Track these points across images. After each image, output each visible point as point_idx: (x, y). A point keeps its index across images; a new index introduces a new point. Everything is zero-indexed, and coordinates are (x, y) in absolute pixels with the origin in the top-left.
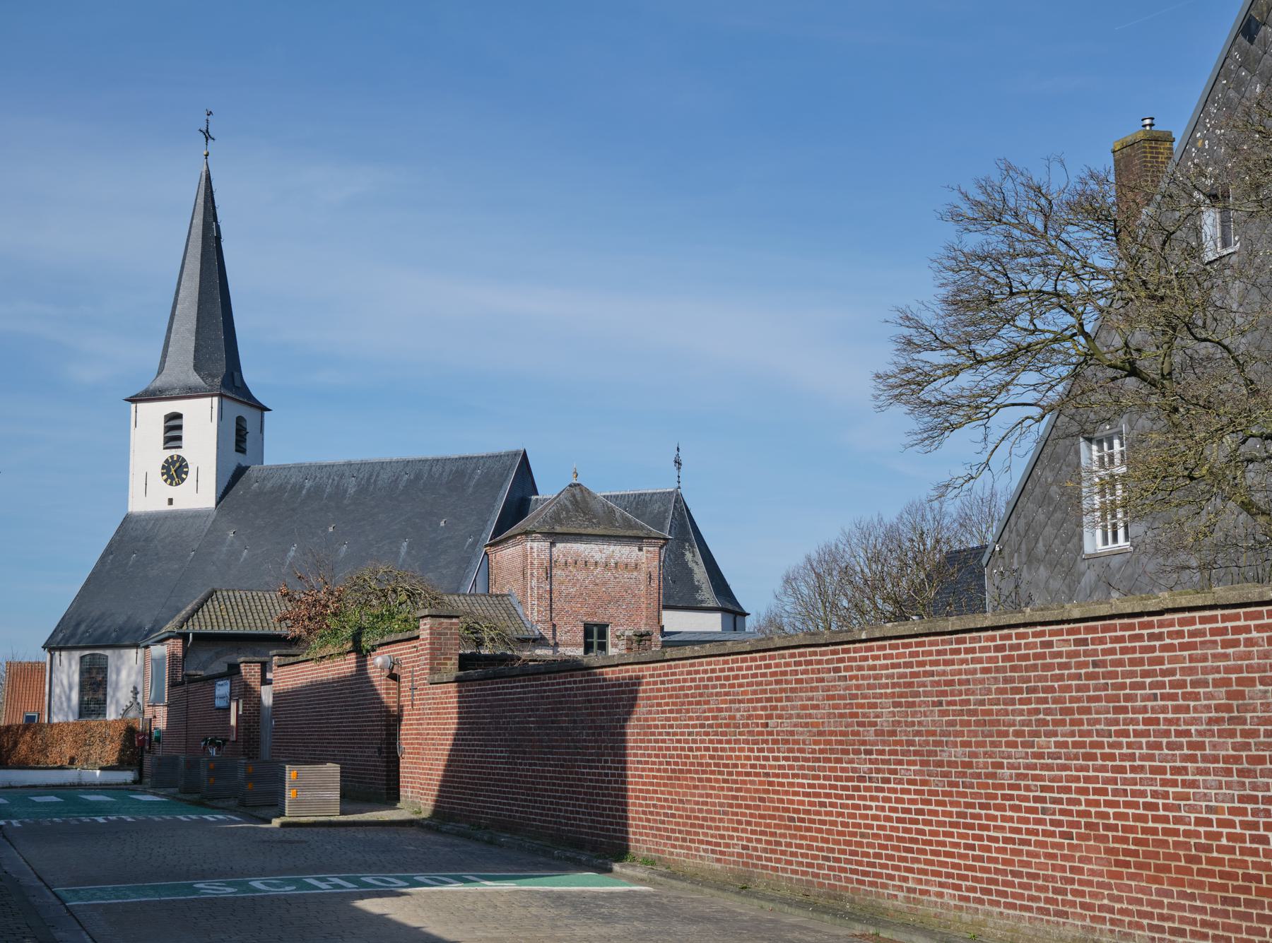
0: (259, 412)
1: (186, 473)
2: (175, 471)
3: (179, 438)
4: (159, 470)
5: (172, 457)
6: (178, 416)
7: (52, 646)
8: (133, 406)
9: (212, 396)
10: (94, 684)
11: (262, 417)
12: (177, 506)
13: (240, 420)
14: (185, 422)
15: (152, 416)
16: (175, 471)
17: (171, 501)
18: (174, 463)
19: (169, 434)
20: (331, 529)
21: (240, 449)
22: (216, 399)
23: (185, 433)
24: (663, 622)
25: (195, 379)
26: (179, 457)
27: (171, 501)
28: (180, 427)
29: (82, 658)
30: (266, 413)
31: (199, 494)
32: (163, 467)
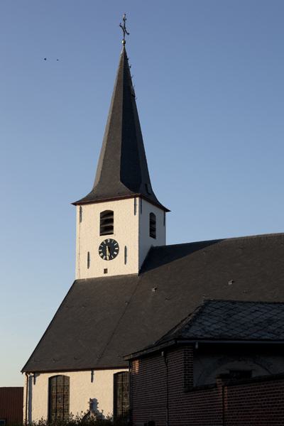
0: (162, 212)
1: (117, 251)
2: (110, 249)
3: (112, 228)
4: (97, 250)
5: (106, 241)
6: (110, 213)
7: (32, 369)
8: (78, 207)
9: (135, 197)
10: (59, 395)
11: (165, 215)
12: (109, 274)
13: (152, 215)
14: (115, 217)
15: (94, 212)
16: (110, 249)
17: (106, 271)
18: (107, 244)
19: (111, 217)
20: (230, 283)
21: (153, 233)
22: (138, 199)
23: (115, 225)
24: (42, 375)
25: (123, 188)
26: (111, 240)
27: (106, 271)
28: (112, 221)
29: (116, 376)
30: (167, 213)
31: (127, 265)
32: (100, 248)
